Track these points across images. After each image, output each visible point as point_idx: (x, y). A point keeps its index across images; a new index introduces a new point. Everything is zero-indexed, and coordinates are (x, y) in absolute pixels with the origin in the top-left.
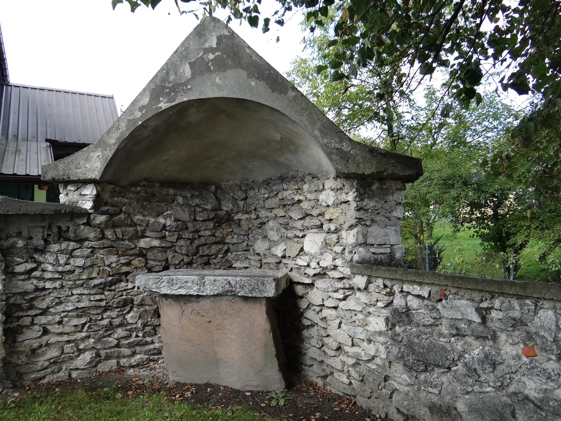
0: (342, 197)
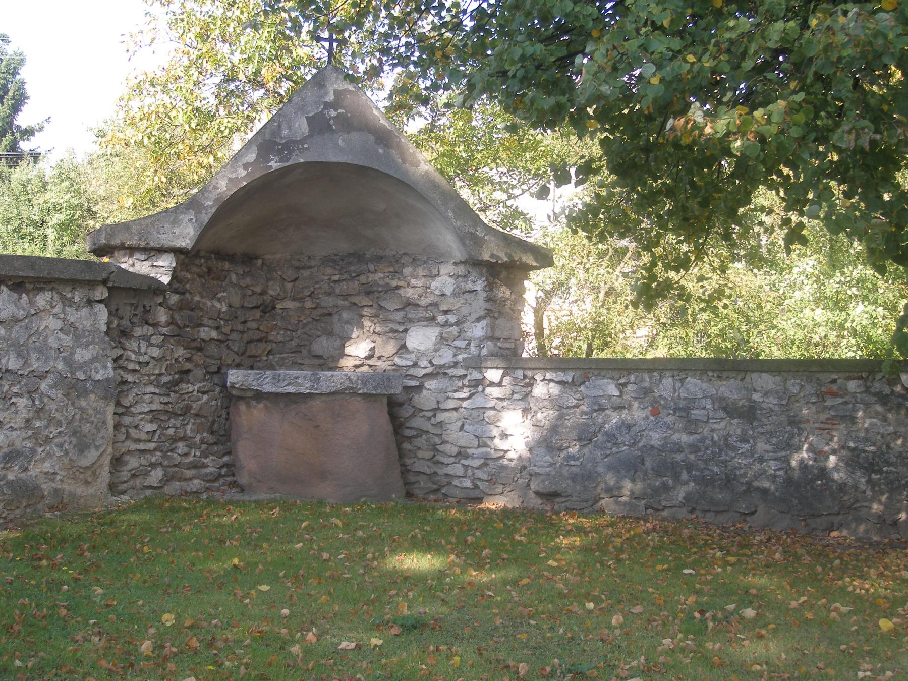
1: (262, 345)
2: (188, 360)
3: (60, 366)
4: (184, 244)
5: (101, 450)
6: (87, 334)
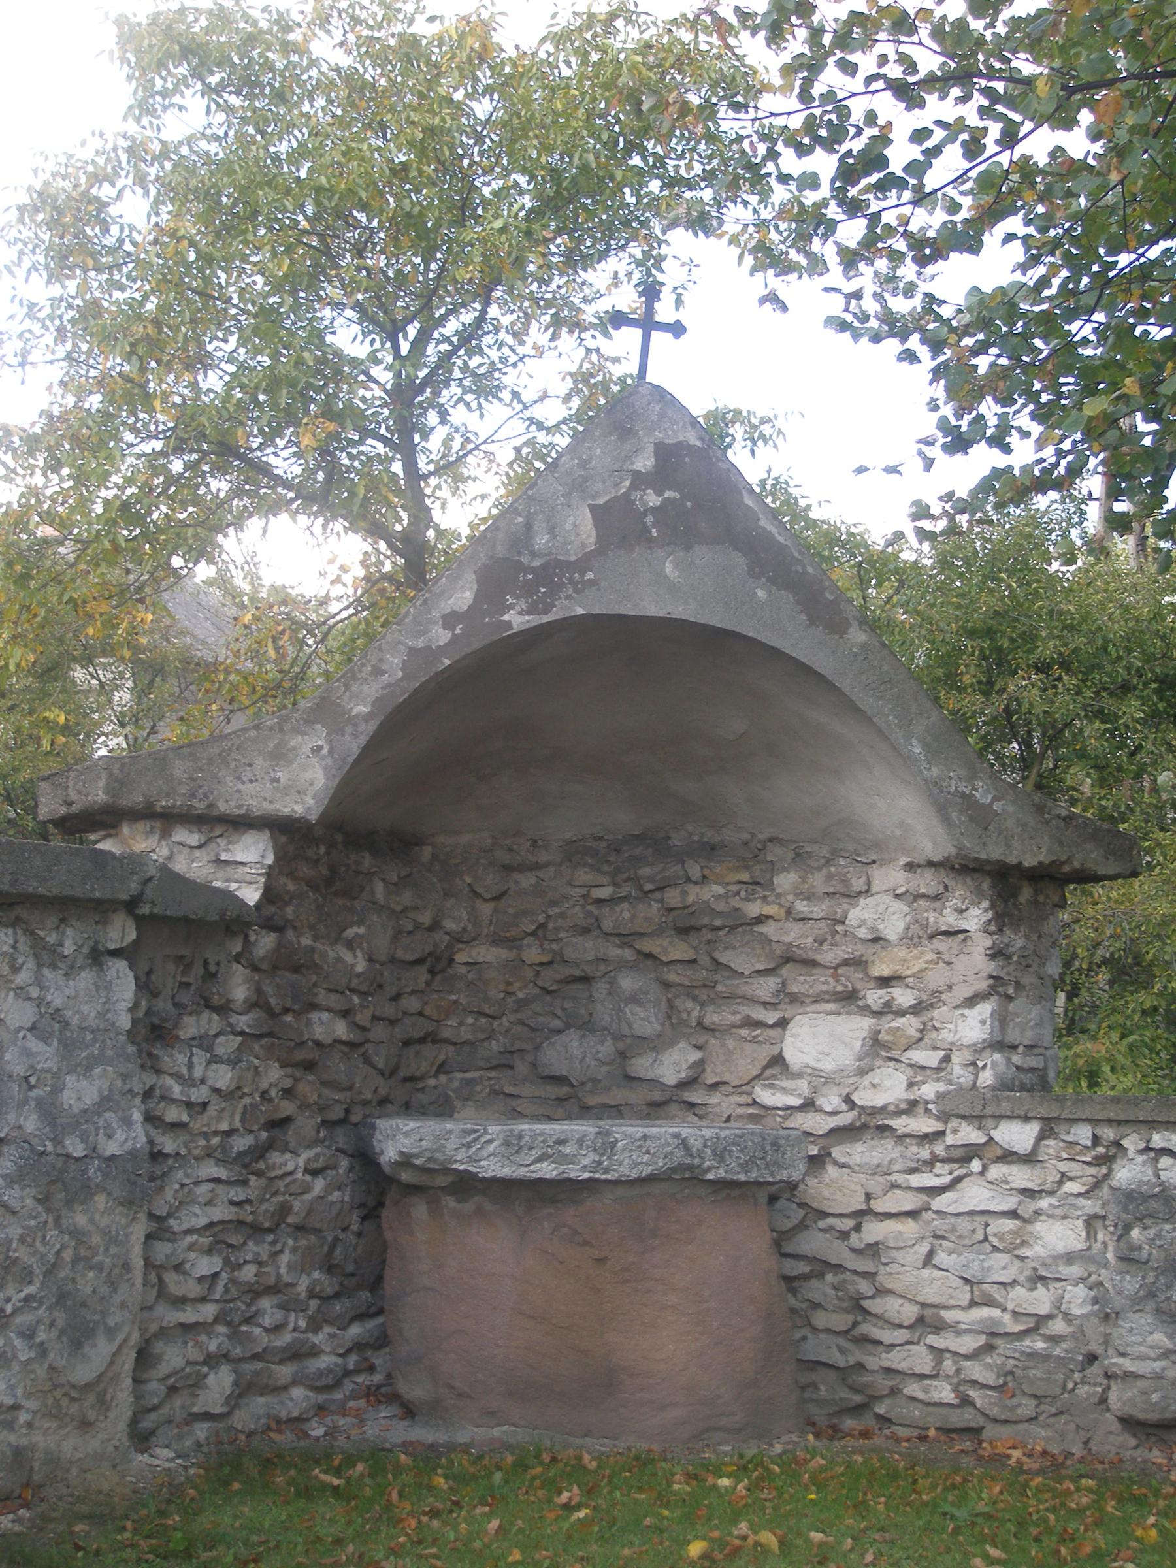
0: (942, 920)
1: (428, 1050)
2: (288, 1093)
3: (31, 1123)
4: (299, 809)
5: (120, 1337)
6: (89, 1037)
